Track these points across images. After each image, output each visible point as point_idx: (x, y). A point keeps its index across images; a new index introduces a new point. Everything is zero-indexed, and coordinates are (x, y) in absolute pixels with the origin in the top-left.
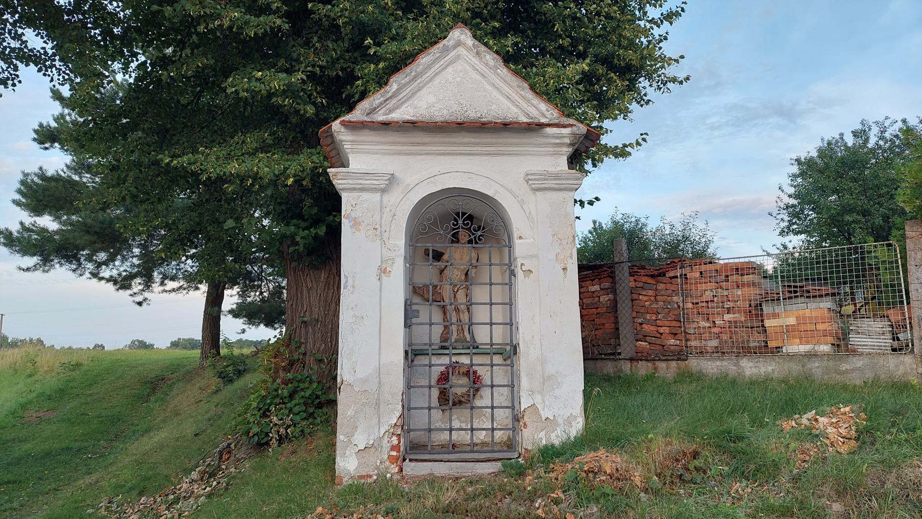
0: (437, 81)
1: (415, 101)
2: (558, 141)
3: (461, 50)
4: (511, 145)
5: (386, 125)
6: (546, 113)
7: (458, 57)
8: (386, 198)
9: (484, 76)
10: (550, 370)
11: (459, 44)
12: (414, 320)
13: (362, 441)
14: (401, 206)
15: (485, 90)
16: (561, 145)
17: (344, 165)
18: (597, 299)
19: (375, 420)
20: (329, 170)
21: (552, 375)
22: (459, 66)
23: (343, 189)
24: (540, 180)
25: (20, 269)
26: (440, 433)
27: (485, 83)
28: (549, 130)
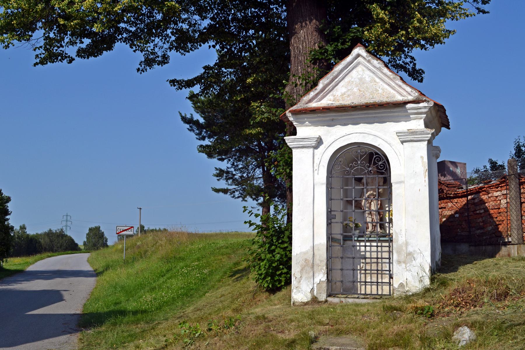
0: (347, 79)
1: (334, 92)
2: (416, 111)
3: (360, 59)
4: (394, 112)
5: (314, 111)
6: (411, 93)
7: (359, 64)
8: (316, 151)
9: (373, 73)
10: (410, 249)
11: (358, 55)
12: (333, 220)
13: (305, 286)
14: (324, 155)
15: (375, 81)
16: (421, 113)
17: (294, 133)
18: (499, 202)
19: (311, 274)
20: (285, 138)
21: (411, 252)
22: (360, 68)
23: (293, 148)
24: (407, 135)
25: (173, 82)
26: (373, 290)
27: (375, 77)
28: (409, 106)
